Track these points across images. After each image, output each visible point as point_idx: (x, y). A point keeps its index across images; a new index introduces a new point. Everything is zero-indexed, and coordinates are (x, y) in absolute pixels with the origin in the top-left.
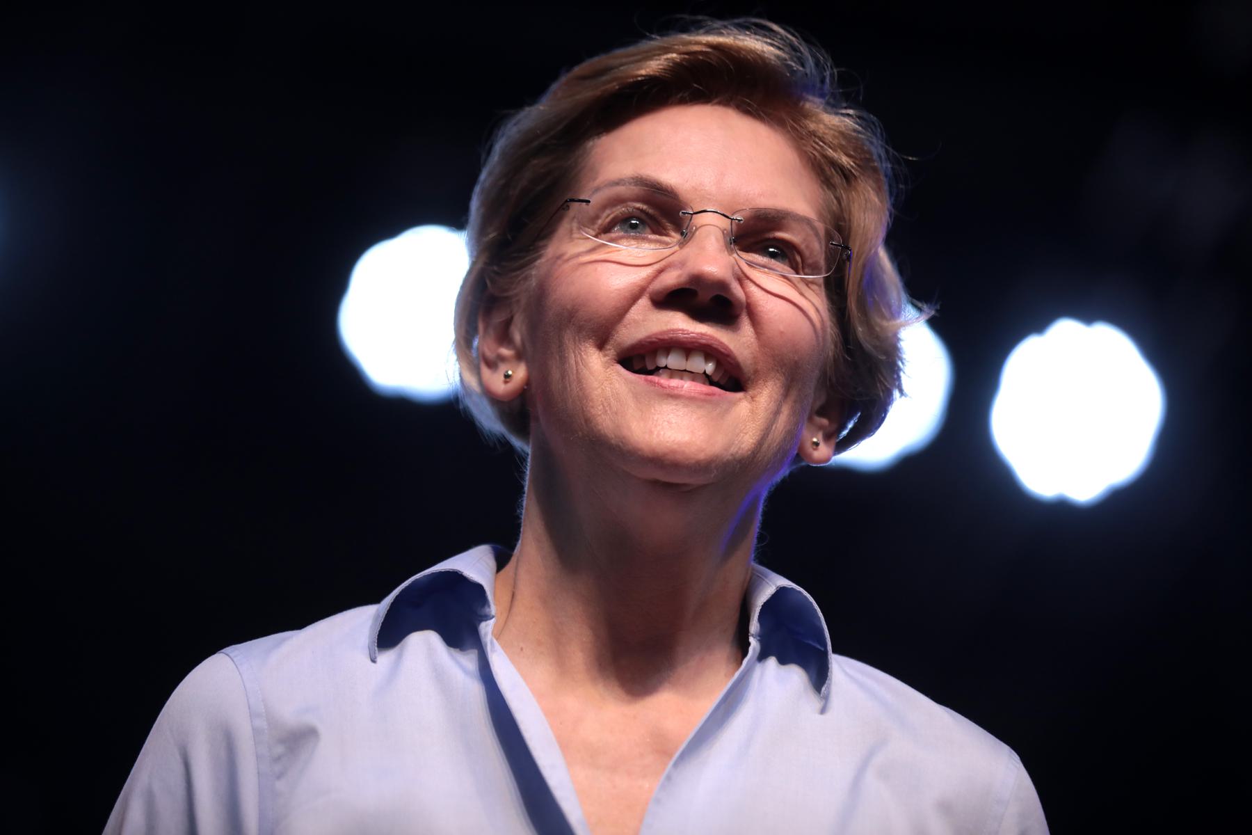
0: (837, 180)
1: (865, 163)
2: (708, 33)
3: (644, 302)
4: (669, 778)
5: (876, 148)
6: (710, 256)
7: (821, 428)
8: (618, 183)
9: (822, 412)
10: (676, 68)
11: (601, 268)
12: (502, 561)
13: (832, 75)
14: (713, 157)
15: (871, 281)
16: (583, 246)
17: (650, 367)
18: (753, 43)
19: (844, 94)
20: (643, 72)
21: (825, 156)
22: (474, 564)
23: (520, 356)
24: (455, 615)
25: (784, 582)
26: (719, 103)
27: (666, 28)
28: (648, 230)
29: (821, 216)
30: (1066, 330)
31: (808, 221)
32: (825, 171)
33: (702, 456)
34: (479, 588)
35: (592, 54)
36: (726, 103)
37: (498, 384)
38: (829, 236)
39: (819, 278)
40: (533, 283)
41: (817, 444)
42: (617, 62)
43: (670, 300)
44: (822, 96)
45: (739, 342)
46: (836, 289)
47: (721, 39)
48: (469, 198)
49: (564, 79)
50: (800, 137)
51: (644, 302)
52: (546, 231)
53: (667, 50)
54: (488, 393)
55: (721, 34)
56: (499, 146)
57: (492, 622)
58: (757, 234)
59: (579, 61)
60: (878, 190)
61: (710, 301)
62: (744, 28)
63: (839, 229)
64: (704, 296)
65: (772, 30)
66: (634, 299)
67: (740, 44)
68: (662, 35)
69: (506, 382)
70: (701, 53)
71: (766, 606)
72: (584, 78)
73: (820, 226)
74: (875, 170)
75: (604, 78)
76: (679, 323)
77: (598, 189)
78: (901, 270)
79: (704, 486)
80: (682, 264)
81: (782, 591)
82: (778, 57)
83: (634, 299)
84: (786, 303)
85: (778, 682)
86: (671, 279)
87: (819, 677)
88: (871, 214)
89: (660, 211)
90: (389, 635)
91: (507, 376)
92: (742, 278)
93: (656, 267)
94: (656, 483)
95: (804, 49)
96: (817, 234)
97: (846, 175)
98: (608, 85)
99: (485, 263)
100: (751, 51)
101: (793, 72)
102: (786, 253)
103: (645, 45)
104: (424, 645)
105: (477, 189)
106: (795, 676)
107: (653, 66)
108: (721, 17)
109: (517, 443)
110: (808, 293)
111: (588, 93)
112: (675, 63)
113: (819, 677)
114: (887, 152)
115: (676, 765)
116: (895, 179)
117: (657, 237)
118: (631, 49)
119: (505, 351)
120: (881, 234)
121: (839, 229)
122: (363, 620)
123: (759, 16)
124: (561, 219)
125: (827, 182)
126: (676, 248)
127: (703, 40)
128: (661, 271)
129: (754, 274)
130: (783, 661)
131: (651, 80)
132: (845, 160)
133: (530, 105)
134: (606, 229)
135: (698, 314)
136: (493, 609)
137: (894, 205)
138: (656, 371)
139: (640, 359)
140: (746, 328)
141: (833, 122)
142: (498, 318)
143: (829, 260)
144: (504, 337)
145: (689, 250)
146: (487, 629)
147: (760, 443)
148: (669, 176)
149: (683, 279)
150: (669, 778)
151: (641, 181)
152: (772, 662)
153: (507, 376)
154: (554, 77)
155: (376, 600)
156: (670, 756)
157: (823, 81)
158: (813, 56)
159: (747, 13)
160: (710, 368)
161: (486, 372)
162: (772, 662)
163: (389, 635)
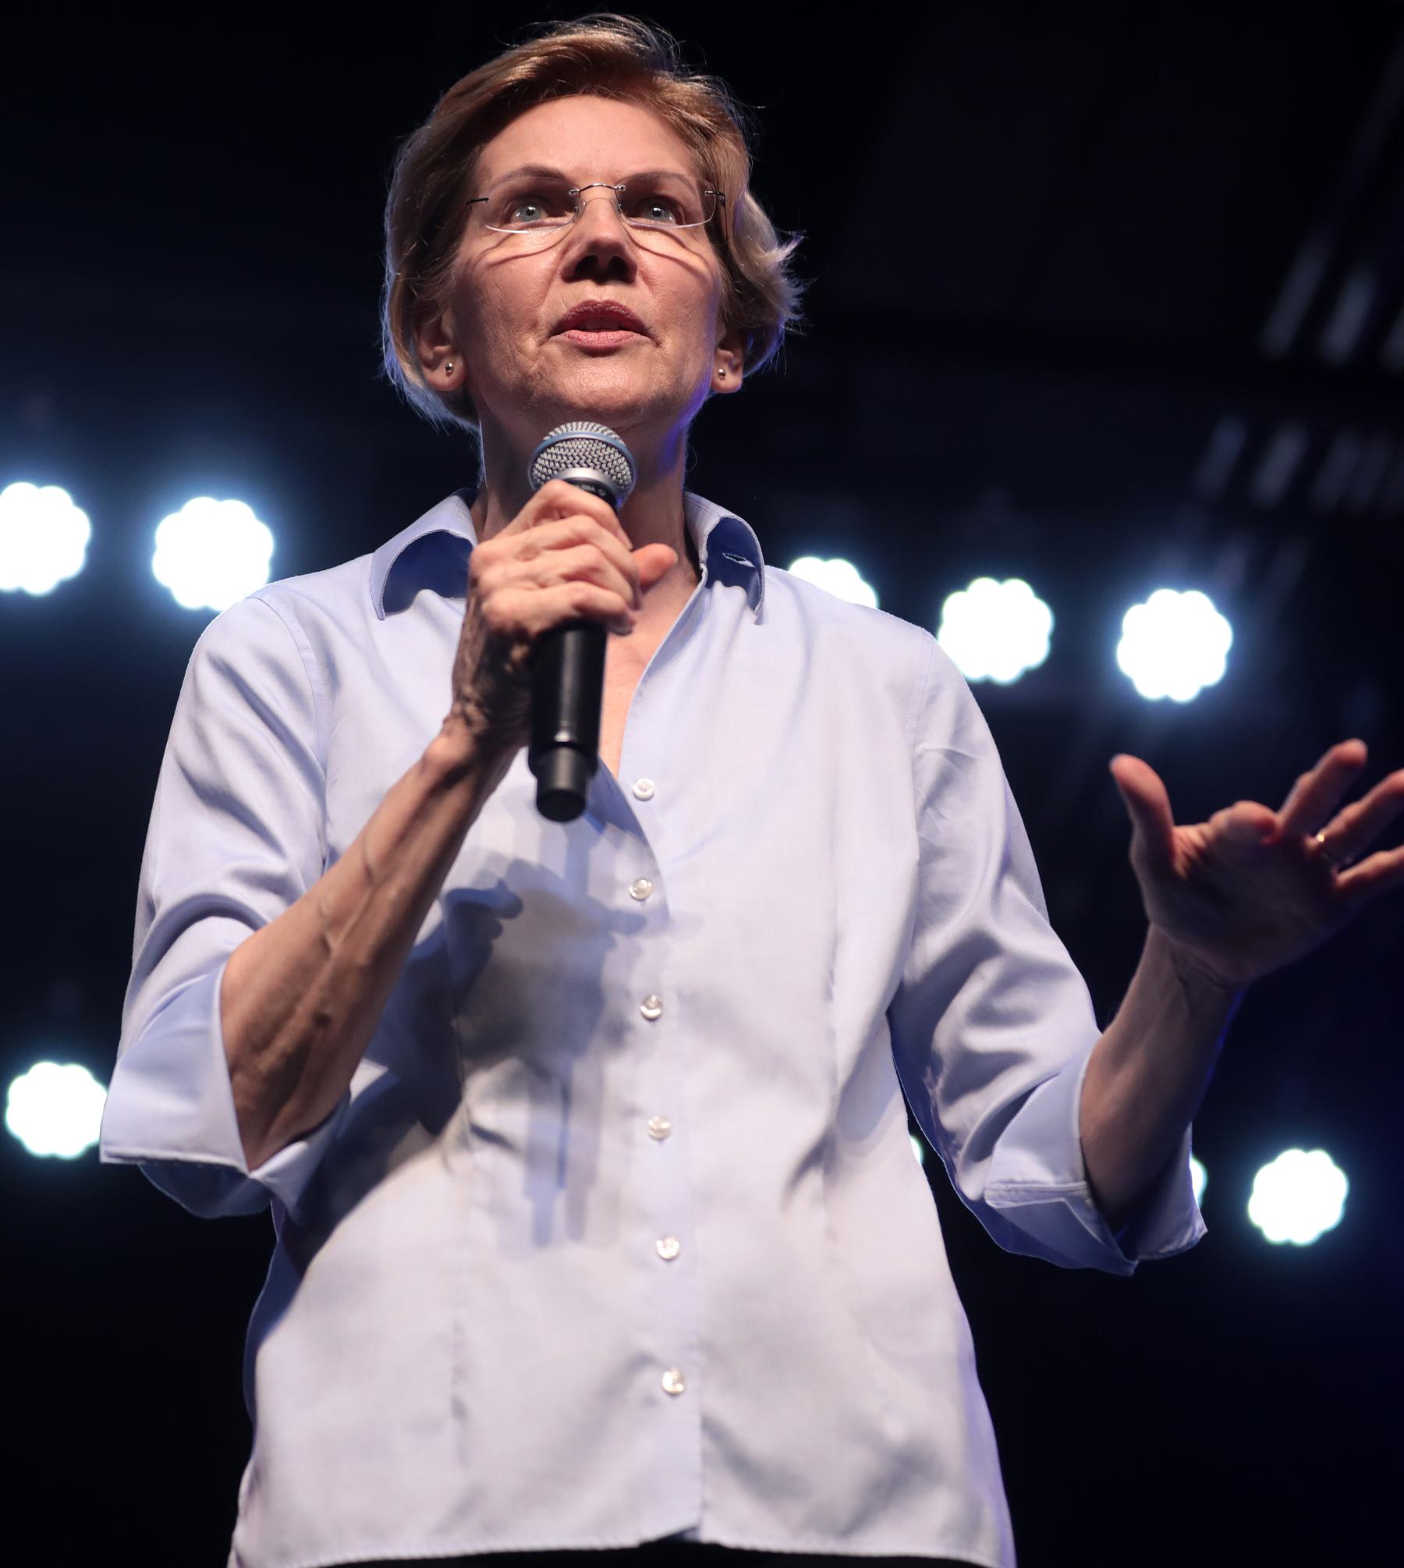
0: (699, 139)
1: (721, 123)
2: (561, 33)
3: (558, 281)
4: (640, 693)
5: (727, 105)
6: (602, 222)
7: (727, 360)
8: (509, 177)
9: (723, 345)
10: (540, 70)
11: (514, 266)
13: (676, 49)
14: (589, 138)
15: (743, 225)
18: (605, 36)
19: (690, 63)
20: (511, 78)
21: (685, 120)
22: (448, 517)
23: (454, 352)
26: (584, 93)
28: (543, 213)
29: (692, 172)
31: (680, 177)
32: (685, 133)
33: (627, 397)
35: (463, 74)
36: (586, 92)
37: (440, 377)
38: (702, 188)
39: (701, 224)
41: (723, 374)
42: (489, 73)
44: (671, 70)
46: (716, 234)
47: (573, 37)
49: (443, 100)
50: (663, 108)
52: (456, 234)
53: (528, 56)
55: (572, 32)
56: (400, 168)
58: (640, 198)
59: (455, 81)
60: (735, 141)
61: (605, 263)
62: (591, 23)
63: (708, 179)
64: (604, 261)
65: (614, 21)
67: (590, 37)
68: (521, 44)
69: (448, 375)
70: (559, 51)
71: (711, 535)
72: (460, 95)
73: (693, 181)
74: (729, 124)
75: (478, 91)
76: (590, 292)
77: (494, 186)
79: (634, 426)
81: (724, 521)
82: (626, 42)
83: (550, 281)
85: (727, 599)
86: (574, 253)
88: (732, 158)
89: (550, 195)
91: (448, 368)
93: (559, 248)
95: (648, 33)
96: (690, 186)
97: (703, 131)
98: (484, 94)
99: (408, 275)
100: (601, 42)
101: (642, 52)
102: (671, 207)
105: (388, 210)
106: (738, 593)
107: (521, 71)
108: (569, 19)
109: (464, 423)
111: (466, 106)
112: (540, 65)
114: (736, 106)
115: (645, 681)
117: (553, 220)
118: (496, 62)
121: (708, 176)
123: (602, 11)
124: (467, 218)
125: (689, 141)
126: (571, 225)
127: (559, 41)
128: (564, 252)
130: (727, 584)
131: (521, 83)
132: (702, 121)
133: (419, 127)
135: (601, 280)
137: (751, 152)
141: (688, 89)
144: (439, 338)
145: (584, 222)
148: (559, 160)
149: (584, 248)
150: (640, 693)
151: (529, 170)
152: (718, 586)
153: (448, 368)
156: (644, 665)
157: (669, 56)
158: (654, 31)
161: (427, 371)
162: (718, 586)
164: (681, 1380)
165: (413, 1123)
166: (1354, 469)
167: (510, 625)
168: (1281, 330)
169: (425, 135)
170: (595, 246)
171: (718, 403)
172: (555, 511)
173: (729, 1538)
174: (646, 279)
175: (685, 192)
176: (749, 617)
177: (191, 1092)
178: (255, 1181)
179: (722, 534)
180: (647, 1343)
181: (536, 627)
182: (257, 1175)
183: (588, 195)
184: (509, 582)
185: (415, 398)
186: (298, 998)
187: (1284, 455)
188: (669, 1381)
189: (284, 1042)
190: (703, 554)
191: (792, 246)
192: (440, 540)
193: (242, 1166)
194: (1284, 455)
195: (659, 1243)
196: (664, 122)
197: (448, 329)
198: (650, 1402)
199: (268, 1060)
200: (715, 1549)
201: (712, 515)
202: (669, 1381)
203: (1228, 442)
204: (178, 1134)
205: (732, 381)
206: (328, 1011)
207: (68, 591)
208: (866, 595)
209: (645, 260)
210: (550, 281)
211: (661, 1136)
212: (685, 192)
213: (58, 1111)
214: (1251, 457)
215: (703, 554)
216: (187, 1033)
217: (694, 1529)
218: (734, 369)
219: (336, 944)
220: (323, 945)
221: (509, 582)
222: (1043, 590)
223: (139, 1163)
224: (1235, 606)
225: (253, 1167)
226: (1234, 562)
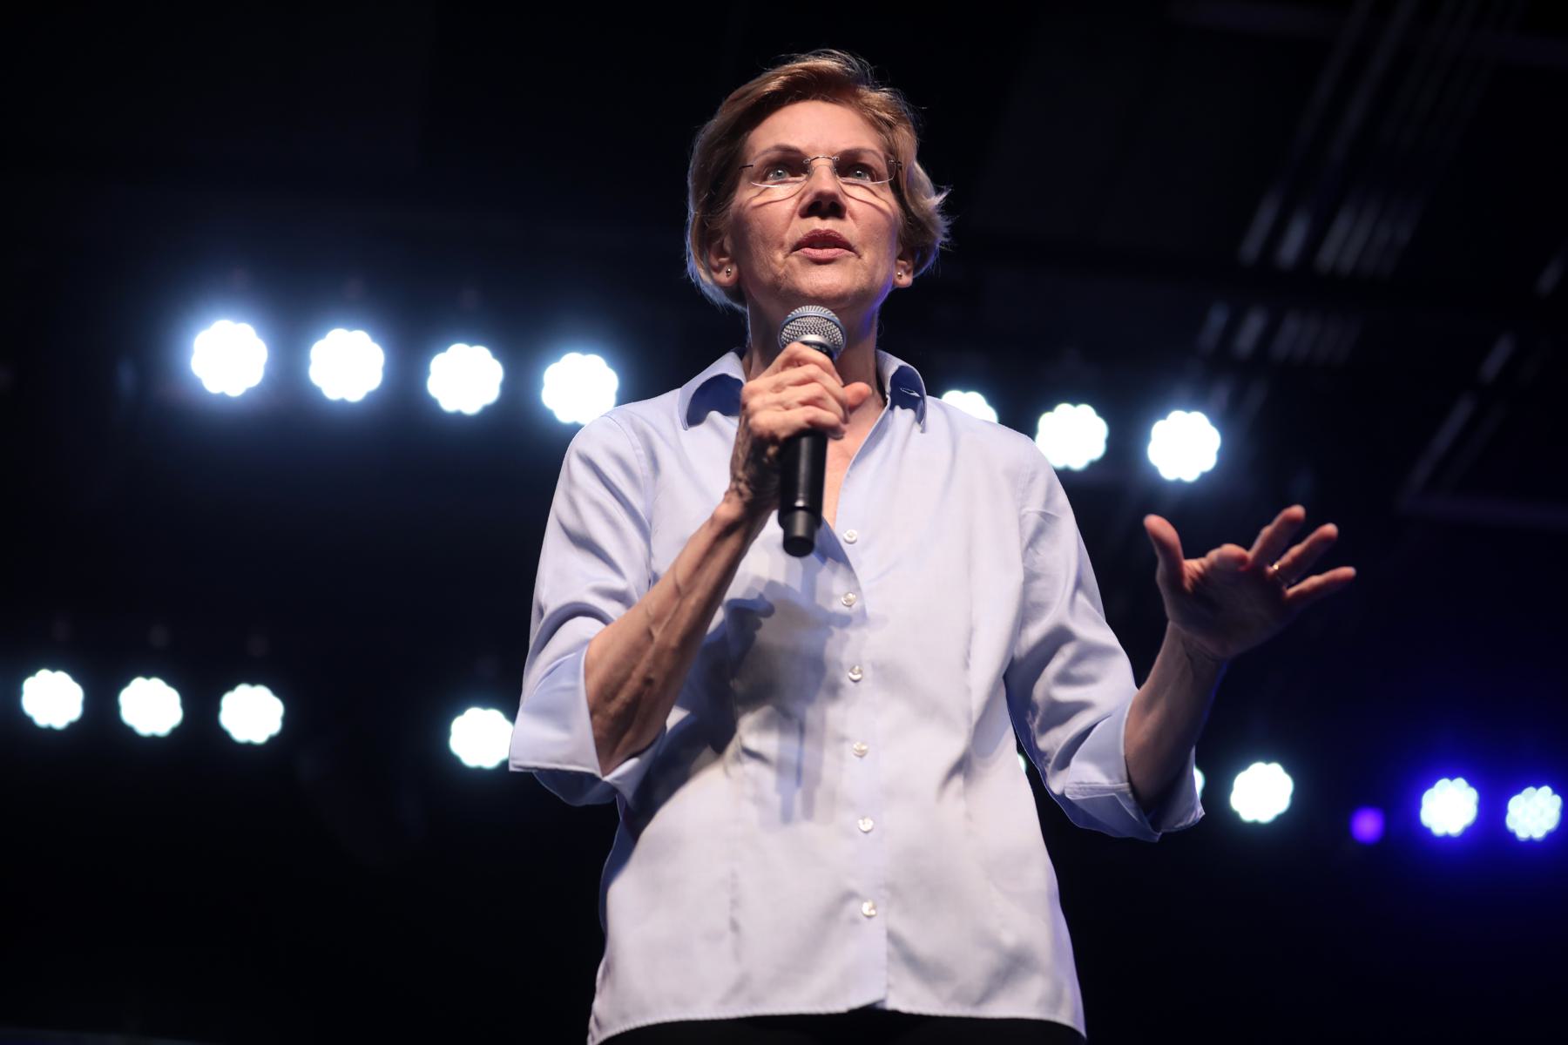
0: (885, 128)
1: (899, 118)
3: (797, 217)
5: (903, 107)
6: (824, 179)
7: (903, 267)
10: (785, 84)
14: (816, 127)
15: (913, 182)
16: (754, 192)
19: (879, 81)
22: (728, 365)
23: (732, 262)
25: (902, 363)
30: (1064, 409)
32: (876, 124)
37: (723, 277)
38: (887, 159)
40: (731, 217)
46: (896, 188)
50: (862, 109)
52: (732, 188)
54: (717, 283)
56: (697, 146)
58: (848, 165)
61: (826, 206)
62: (818, 55)
64: (826, 204)
73: (881, 154)
76: (817, 224)
78: (928, 173)
81: (901, 368)
83: (791, 218)
86: (807, 200)
87: (921, 417)
88: (906, 140)
89: (792, 163)
95: (853, 61)
98: (750, 100)
103: (765, 76)
106: (910, 413)
107: (774, 85)
109: (738, 307)
110: (882, 195)
111: (739, 108)
119: (723, 259)
120: (914, 155)
121: (891, 151)
125: (879, 129)
127: (797, 66)
129: (848, 189)
131: (774, 93)
132: (887, 116)
135: (823, 217)
141: (878, 97)
143: (890, 168)
145: (812, 181)
148: (797, 141)
151: (778, 148)
154: (720, 103)
159: (818, 47)
162: (897, 408)
166: (1299, 335)
167: (767, 433)
168: (1251, 248)
169: (713, 125)
171: (898, 293)
172: (795, 362)
174: (852, 216)
175: (877, 161)
177: (566, 727)
178: (606, 783)
180: (853, 884)
181: (783, 434)
182: (607, 779)
183: (816, 163)
184: (766, 406)
185: (707, 291)
186: (633, 668)
187: (1254, 325)
188: (866, 908)
189: (624, 695)
190: (888, 389)
193: (599, 774)
194: (1254, 325)
196: (864, 117)
197: (728, 247)
198: (855, 921)
199: (614, 707)
200: (896, 1014)
201: (894, 364)
202: (866, 908)
203: (1217, 319)
204: (559, 753)
205: (906, 280)
206: (652, 676)
207: (488, 412)
208: (991, 414)
209: (852, 204)
210: (791, 218)
211: (862, 754)
212: (877, 161)
213: (479, 738)
214: (1231, 330)
215: (888, 389)
216: (564, 689)
217: (882, 1001)
218: (908, 273)
219: (657, 634)
220: (649, 634)
221: (766, 406)
222: (1102, 411)
224: (1223, 421)
225: (605, 773)
226: (1222, 394)
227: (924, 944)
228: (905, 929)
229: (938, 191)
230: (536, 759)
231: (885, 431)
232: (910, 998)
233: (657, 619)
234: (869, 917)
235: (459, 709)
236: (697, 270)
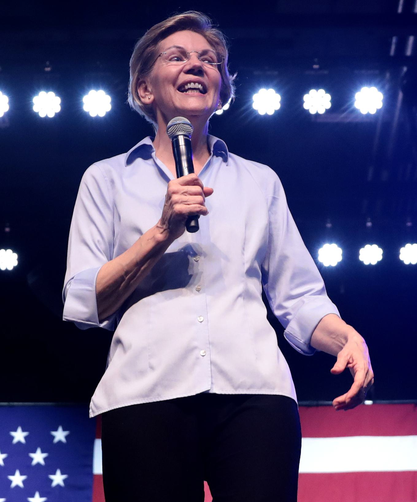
6: (194, 61)
12: (153, 140)
17: (186, 87)
18: (193, 15)
22: (147, 141)
23: (151, 94)
24: (145, 153)
27: (171, 16)
34: (150, 146)
36: (190, 30)
43: (189, 72)
45: (204, 79)
48: (50, 402)
51: (182, 73)
56: (130, 65)
57: (154, 153)
61: (198, 71)
64: (196, 71)
66: (180, 73)
76: (191, 77)
80: (190, 64)
81: (218, 141)
83: (180, 73)
84: (212, 71)
85: (217, 161)
86: (188, 68)
87: (225, 160)
89: (182, 54)
90: (129, 161)
92: (203, 65)
94: (192, 116)
104: (139, 161)
106: (220, 159)
111: (159, 31)
113: (225, 160)
116: (227, 44)
122: (123, 158)
130: (217, 156)
131: (127, 98)
134: (170, 60)
135: (195, 74)
136: (154, 149)
138: (186, 90)
139: (182, 88)
140: (206, 77)
141: (212, 32)
142: (143, 85)
145: (190, 61)
146: (153, 154)
147: (212, 106)
155: (126, 151)
160: (200, 86)
162: (215, 156)
163: (129, 161)
164: (205, 352)
165: (71, 323)
170: (195, 66)
173: (218, 392)
176: (224, 164)
179: (218, 146)
180: (195, 343)
183: (191, 54)
190: (212, 149)
191: (235, 76)
192: (144, 146)
195: (199, 318)
198: (198, 358)
200: (215, 395)
201: (214, 140)
202: (202, 353)
214: (402, 46)
215: (212, 149)
217: (209, 390)
223: (249, 104)
227: (226, 366)
228: (216, 358)
229: (232, 73)
230: (133, 398)
231: (90, 222)
232: (221, 388)
233: (127, 273)
234: (203, 356)
235: (97, 119)
236: (130, 100)
